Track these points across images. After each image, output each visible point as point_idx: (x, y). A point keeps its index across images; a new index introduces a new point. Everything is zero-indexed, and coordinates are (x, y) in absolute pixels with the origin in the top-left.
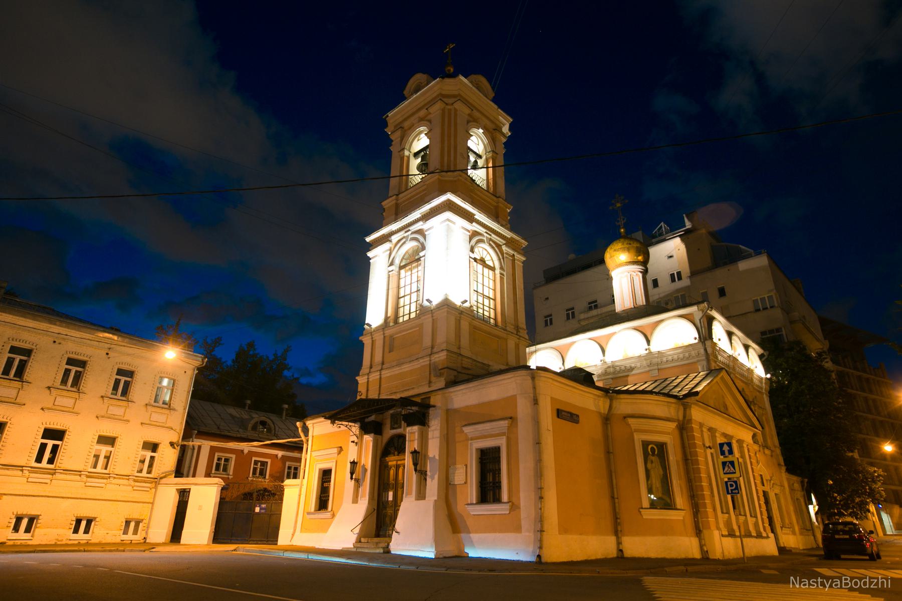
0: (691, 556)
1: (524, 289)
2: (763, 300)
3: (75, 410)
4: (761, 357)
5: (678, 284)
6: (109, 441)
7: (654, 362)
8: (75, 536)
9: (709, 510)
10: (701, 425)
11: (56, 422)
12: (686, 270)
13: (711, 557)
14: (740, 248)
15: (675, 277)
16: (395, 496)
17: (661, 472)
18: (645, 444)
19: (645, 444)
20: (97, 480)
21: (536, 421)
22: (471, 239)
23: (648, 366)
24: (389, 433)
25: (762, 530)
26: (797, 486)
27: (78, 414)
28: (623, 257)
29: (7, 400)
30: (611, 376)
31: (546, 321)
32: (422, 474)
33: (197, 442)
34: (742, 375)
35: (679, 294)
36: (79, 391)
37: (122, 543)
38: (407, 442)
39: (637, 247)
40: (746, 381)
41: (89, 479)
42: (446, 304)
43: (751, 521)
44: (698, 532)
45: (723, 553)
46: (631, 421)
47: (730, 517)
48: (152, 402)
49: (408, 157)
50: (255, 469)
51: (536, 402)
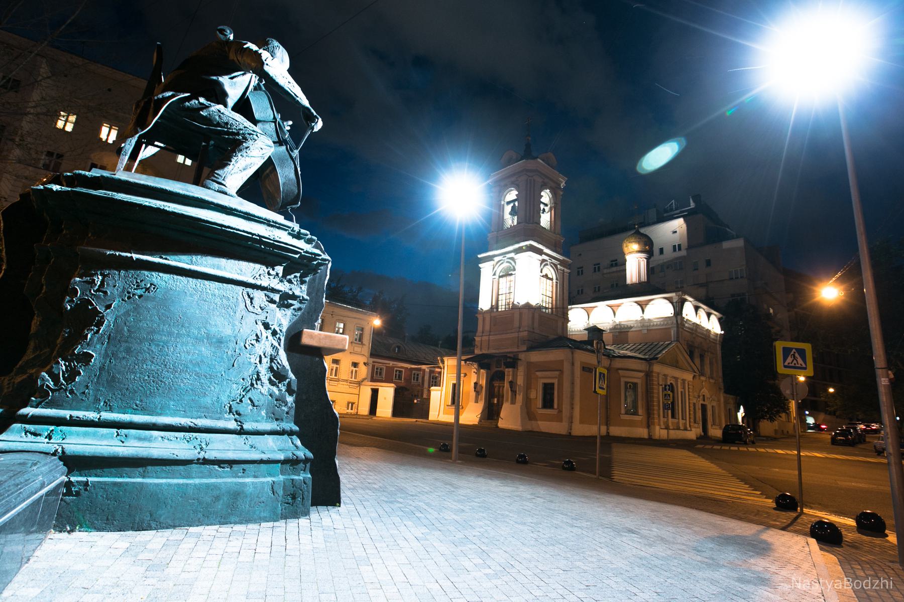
0: (642, 437)
4: (720, 320)
5: (678, 254)
7: (646, 327)
9: (656, 416)
10: (658, 374)
12: (685, 244)
16: (498, 401)
19: (626, 383)
21: (573, 373)
22: (541, 264)
23: (642, 327)
24: (494, 369)
25: (688, 426)
26: (731, 401)
28: (635, 247)
30: (618, 331)
31: (578, 272)
32: (514, 392)
34: (703, 334)
37: (347, 414)
38: (506, 376)
40: (704, 337)
41: (331, 382)
42: (528, 306)
43: (681, 422)
44: (648, 427)
45: (660, 436)
46: (620, 371)
47: (668, 420)
49: (503, 205)
50: (414, 378)
51: (573, 364)
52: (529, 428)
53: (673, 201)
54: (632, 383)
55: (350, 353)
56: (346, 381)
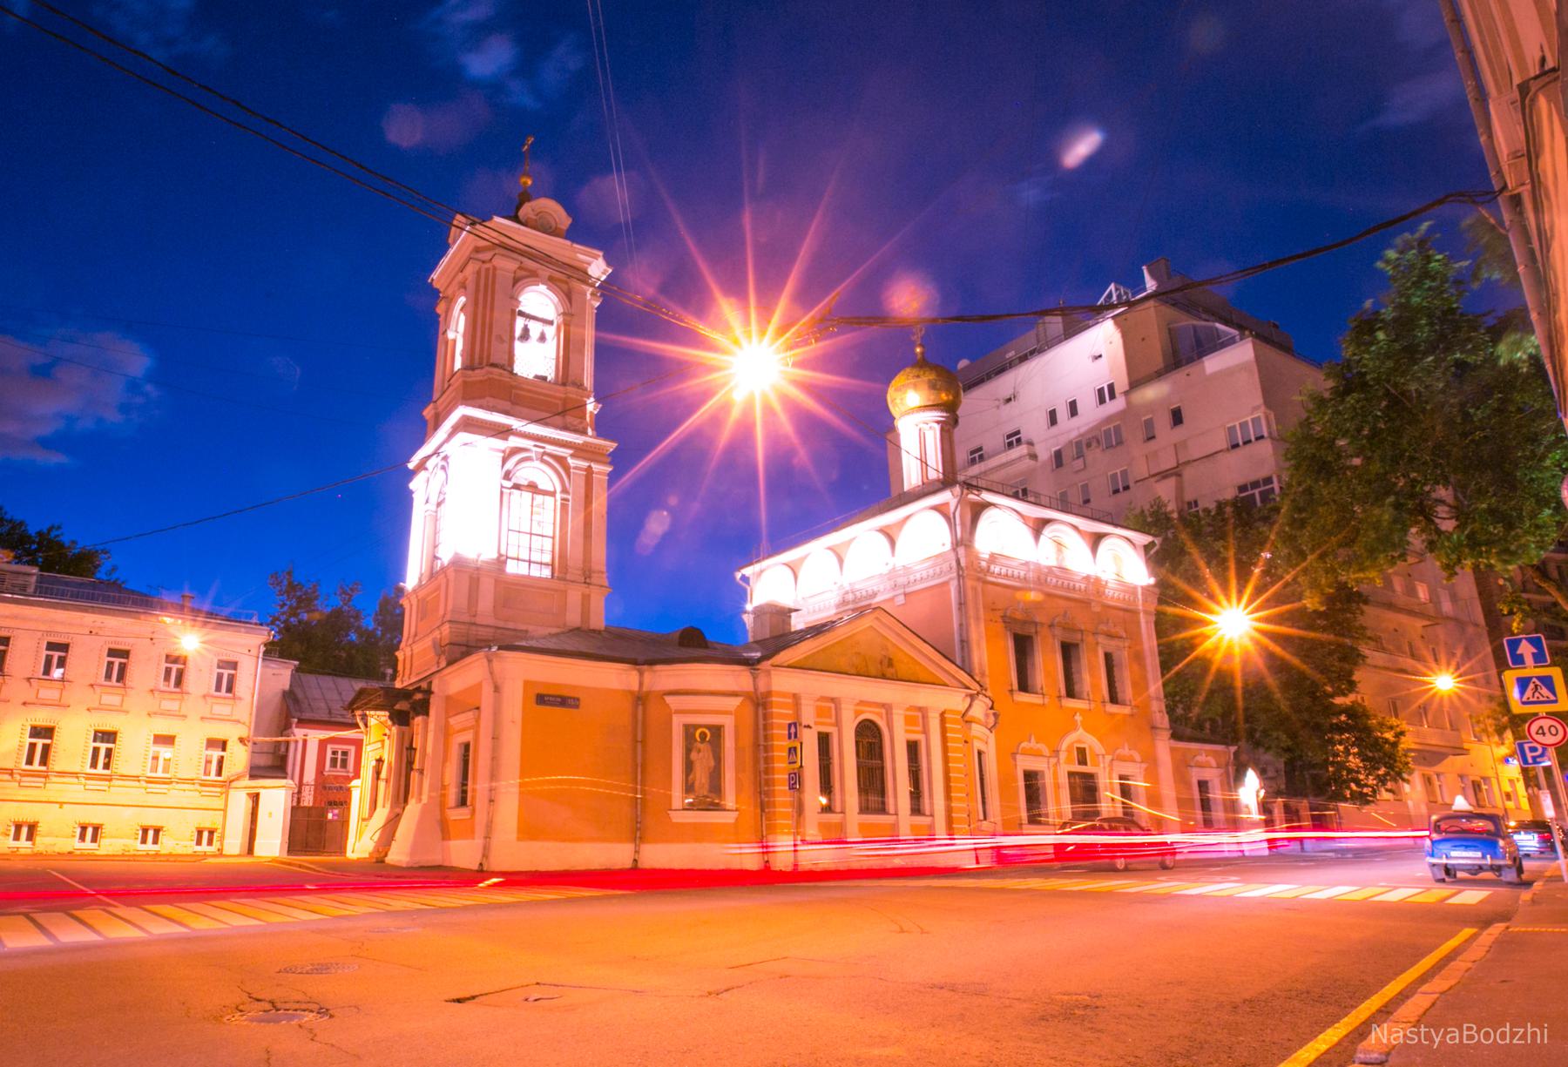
1: (608, 513)
2: (1244, 426)
3: (124, 708)
6: (167, 740)
8: (144, 847)
11: (108, 722)
12: (1122, 384)
13: (773, 868)
14: (1217, 329)
15: (1105, 394)
17: (712, 763)
18: (689, 730)
19: (689, 730)
20: (158, 786)
22: (504, 461)
27: (127, 712)
29: (50, 702)
30: (851, 606)
33: (299, 733)
35: (1111, 426)
36: (125, 687)
39: (929, 381)
41: (24, 779)
46: (668, 699)
48: (213, 691)
52: (435, 858)
53: (1112, 287)
54: (709, 727)
55: (149, 715)
56: (191, 781)
